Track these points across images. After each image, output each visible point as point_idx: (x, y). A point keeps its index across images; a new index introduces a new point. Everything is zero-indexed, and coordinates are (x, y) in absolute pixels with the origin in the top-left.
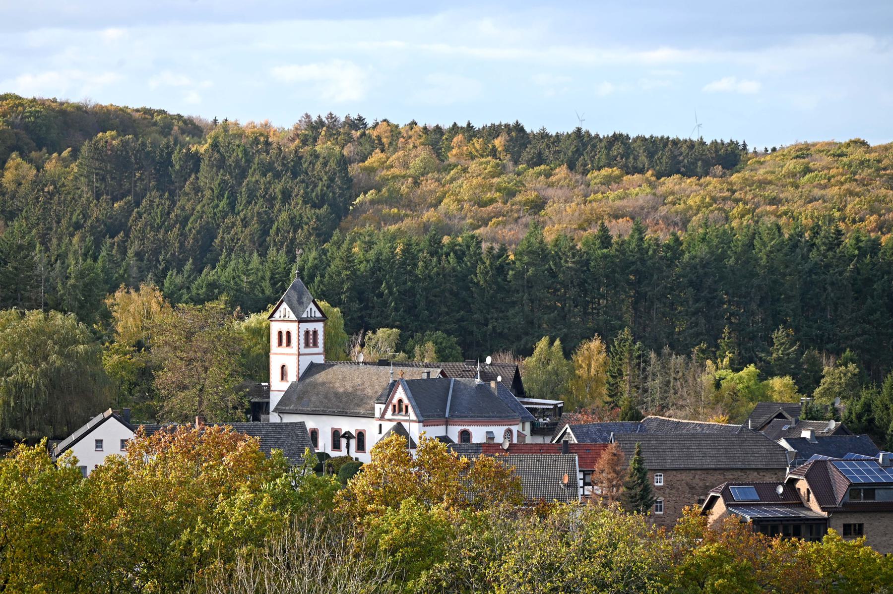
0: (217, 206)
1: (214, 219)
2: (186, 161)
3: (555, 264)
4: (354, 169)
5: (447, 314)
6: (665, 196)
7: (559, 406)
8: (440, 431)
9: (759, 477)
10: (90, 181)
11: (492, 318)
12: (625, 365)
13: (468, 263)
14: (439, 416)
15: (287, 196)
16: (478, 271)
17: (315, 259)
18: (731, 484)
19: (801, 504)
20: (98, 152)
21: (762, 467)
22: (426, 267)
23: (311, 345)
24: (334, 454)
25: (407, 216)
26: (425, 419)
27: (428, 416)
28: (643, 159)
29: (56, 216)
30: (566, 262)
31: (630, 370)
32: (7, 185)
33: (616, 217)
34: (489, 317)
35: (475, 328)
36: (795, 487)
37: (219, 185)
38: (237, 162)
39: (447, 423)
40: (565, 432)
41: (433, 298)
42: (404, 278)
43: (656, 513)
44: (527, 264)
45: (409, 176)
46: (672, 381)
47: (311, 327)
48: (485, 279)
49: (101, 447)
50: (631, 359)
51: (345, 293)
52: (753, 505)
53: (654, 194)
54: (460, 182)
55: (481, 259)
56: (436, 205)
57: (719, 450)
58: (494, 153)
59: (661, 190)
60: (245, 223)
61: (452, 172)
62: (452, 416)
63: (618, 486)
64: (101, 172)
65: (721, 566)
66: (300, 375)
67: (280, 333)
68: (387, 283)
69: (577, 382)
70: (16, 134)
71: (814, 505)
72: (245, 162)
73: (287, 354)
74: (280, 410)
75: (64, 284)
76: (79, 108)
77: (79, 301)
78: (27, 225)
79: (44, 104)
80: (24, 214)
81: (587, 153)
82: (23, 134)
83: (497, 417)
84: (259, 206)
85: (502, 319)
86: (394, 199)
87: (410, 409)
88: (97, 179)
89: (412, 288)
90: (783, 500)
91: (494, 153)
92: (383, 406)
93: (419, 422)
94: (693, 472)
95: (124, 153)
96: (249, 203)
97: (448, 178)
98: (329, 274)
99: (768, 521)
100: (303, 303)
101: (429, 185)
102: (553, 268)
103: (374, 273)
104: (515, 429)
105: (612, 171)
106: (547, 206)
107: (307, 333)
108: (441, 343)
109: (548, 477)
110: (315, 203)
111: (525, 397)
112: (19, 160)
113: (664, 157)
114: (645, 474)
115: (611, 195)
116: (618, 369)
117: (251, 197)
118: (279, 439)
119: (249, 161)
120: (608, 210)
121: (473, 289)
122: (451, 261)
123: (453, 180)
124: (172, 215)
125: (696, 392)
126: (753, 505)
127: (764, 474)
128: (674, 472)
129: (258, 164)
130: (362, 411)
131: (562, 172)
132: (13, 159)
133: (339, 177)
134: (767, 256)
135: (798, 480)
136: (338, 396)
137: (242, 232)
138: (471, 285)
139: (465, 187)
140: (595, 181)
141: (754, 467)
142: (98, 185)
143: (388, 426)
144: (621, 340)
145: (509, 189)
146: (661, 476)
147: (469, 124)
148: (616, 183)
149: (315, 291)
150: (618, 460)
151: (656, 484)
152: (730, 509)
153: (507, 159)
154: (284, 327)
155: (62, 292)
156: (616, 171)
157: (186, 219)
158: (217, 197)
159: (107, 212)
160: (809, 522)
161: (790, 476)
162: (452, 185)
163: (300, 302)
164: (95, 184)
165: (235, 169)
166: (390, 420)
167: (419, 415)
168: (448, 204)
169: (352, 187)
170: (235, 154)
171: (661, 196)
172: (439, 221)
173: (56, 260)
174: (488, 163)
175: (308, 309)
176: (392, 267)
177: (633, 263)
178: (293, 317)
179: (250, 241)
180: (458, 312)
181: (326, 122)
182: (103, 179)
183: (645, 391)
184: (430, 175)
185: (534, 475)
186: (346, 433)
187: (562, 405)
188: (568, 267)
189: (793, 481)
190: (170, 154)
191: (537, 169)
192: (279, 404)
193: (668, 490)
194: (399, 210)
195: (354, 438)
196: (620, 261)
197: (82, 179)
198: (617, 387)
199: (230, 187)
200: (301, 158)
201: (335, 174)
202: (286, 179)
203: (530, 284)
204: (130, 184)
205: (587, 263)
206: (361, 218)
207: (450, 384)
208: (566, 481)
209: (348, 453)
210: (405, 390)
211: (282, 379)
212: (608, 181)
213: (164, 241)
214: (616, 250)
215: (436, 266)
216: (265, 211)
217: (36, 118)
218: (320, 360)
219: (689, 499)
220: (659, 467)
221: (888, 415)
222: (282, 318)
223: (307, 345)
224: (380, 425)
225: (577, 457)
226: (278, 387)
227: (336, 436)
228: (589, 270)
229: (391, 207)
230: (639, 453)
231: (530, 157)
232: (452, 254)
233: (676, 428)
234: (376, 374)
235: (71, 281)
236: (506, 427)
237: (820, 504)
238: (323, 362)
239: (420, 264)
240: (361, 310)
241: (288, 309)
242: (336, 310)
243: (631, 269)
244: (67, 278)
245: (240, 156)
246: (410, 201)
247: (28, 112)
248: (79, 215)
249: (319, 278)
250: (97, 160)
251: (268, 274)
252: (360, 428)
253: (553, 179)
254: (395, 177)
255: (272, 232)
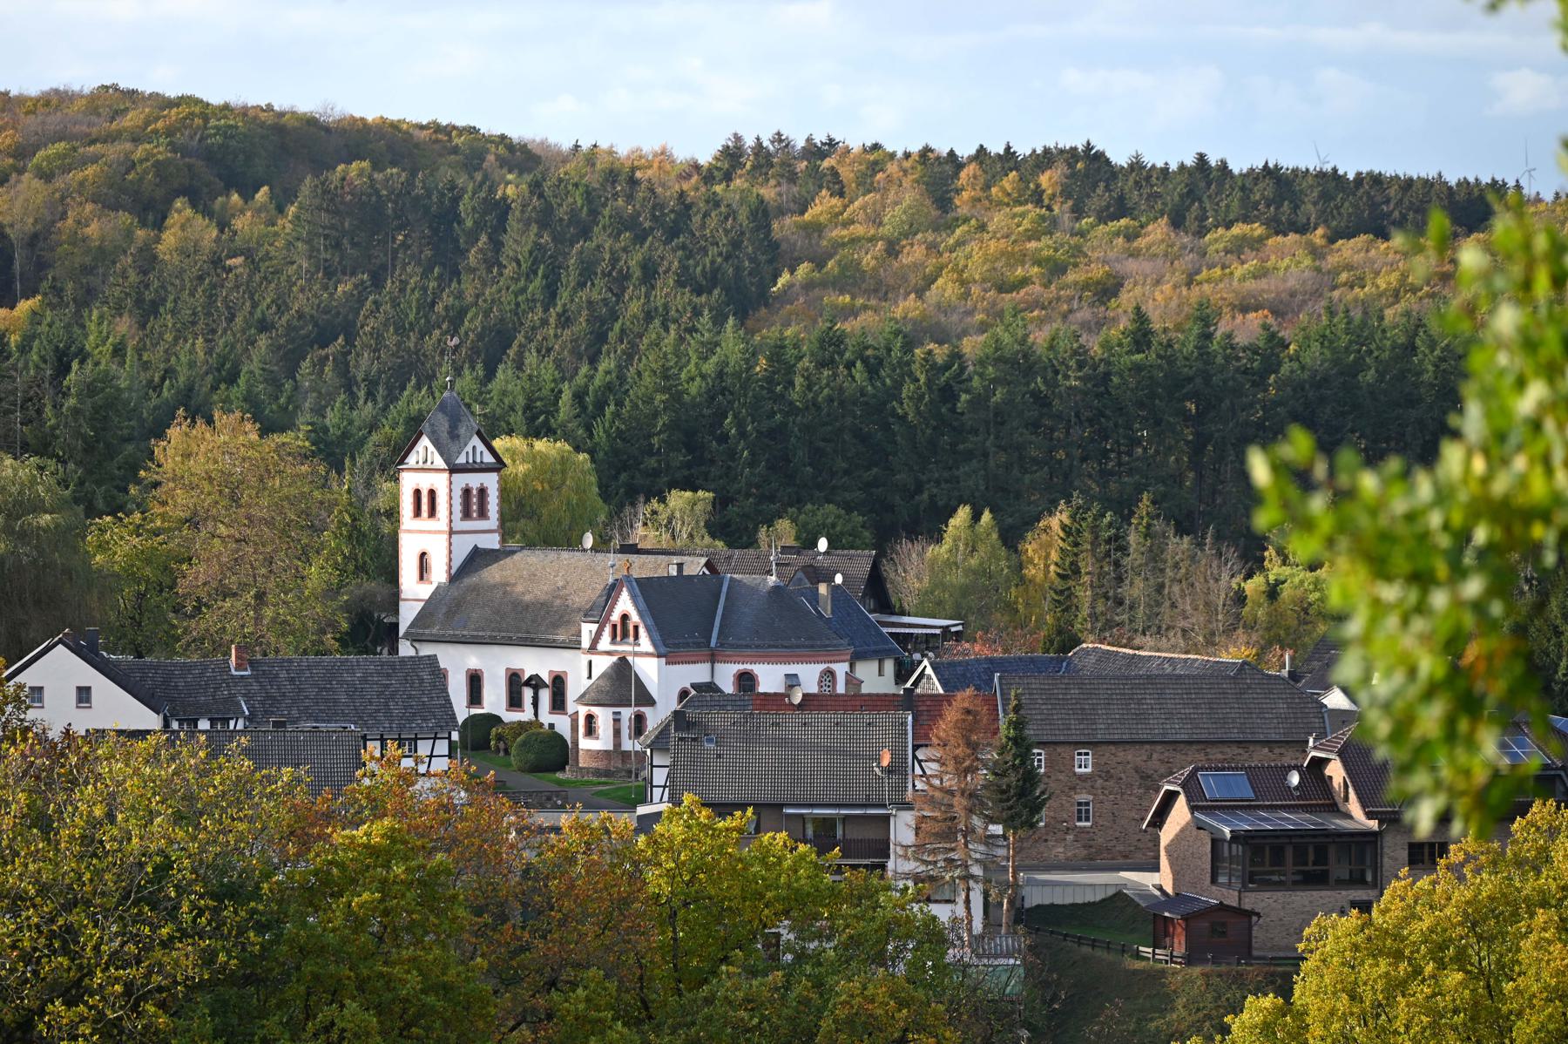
0: (523, 290)
1: (516, 314)
2: (485, 213)
3: (1045, 381)
4: (783, 228)
5: (847, 472)
6: (1335, 272)
7: (953, 629)
8: (697, 673)
9: (1273, 756)
10: (312, 249)
11: (929, 481)
12: (1084, 554)
13: (888, 381)
14: (698, 645)
15: (650, 272)
16: (903, 396)
17: (608, 373)
18: (1202, 769)
19: (1333, 807)
20: (329, 199)
21: (1277, 738)
22: (809, 388)
23: (475, 515)
24: (510, 717)
25: (865, 308)
26: (671, 649)
27: (677, 646)
28: (1309, 209)
29: (228, 308)
30: (1067, 377)
31: (1093, 564)
32: (167, 257)
33: (1245, 309)
34: (924, 478)
35: (897, 499)
36: (1323, 774)
37: (531, 253)
38: (573, 213)
39: (713, 659)
40: (922, 674)
41: (822, 444)
42: (768, 405)
43: (1078, 824)
44: (993, 381)
45: (882, 239)
46: (1167, 584)
47: (474, 480)
48: (917, 408)
49: (88, 700)
50: (1095, 543)
51: (659, 433)
52: (1241, 808)
53: (1318, 270)
54: (968, 249)
55: (911, 374)
56: (920, 293)
57: (1197, 707)
58: (1037, 197)
59: (1332, 260)
60: (565, 320)
61: (958, 232)
62: (722, 645)
63: (972, 770)
64: (334, 233)
65: (388, 867)
66: (453, 572)
67: (417, 493)
68: (735, 417)
69: (1026, 590)
70: (190, 167)
71: (1354, 807)
72: (588, 215)
73: (429, 532)
74: (415, 639)
75: (56, 406)
76: (311, 122)
77: (84, 437)
78: (174, 325)
79: (245, 114)
80: (169, 305)
81: (1210, 197)
82: (199, 164)
83: (807, 647)
84: (597, 292)
85: (947, 481)
86: (850, 279)
87: (642, 632)
88: (325, 246)
89: (784, 425)
90: (1299, 798)
91: (1037, 197)
92: (594, 627)
93: (659, 656)
94: (1148, 747)
95: (374, 199)
96: (582, 285)
97: (951, 241)
98: (631, 401)
99: (1264, 837)
100: (458, 436)
101: (914, 254)
102: (1043, 388)
103: (713, 398)
104: (841, 669)
105: (1252, 229)
106: (1123, 290)
107: (467, 492)
108: (834, 526)
109: (853, 755)
110: (701, 286)
111: (893, 613)
112: (189, 212)
113: (1347, 204)
114: (1029, 749)
115: (1239, 271)
116: (1072, 563)
117: (587, 274)
118: (387, 686)
119: (594, 213)
120: (1230, 296)
121: (895, 428)
122: (858, 376)
123: (960, 243)
124: (439, 308)
125: (1207, 604)
126: (1241, 808)
127: (1283, 751)
128: (1112, 747)
129: (610, 217)
130: (561, 637)
131: (1158, 231)
132: (179, 211)
133: (749, 240)
134: (1437, 366)
135: (1328, 760)
136: (521, 608)
137: (556, 336)
138: (891, 420)
139: (977, 256)
140: (1216, 246)
141: (1262, 737)
142: (328, 257)
143: (602, 664)
144: (1078, 508)
145: (1055, 261)
146: (1087, 754)
147: (1008, 148)
148: (1252, 249)
149: (605, 431)
150: (976, 722)
151: (1077, 770)
152: (1196, 814)
153: (1061, 209)
154: (425, 481)
155: (53, 421)
156: (1258, 229)
157: (462, 313)
158: (528, 275)
159: (321, 302)
160: (1344, 839)
161: (1314, 753)
162: (954, 255)
163: (454, 436)
164: (323, 255)
165: (568, 226)
166: (609, 653)
167: (660, 643)
168: (945, 288)
169: (776, 256)
170: (570, 200)
171: (1329, 272)
172: (924, 317)
173: (163, 379)
174: (1023, 215)
175: (469, 448)
176: (744, 387)
177: (1190, 379)
178: (439, 462)
179: (572, 352)
180: (868, 468)
181: (771, 148)
182: (337, 246)
183: (1119, 602)
184: (919, 236)
185: (828, 751)
186: (531, 678)
187: (960, 628)
188: (1070, 388)
189: (1319, 764)
190: (456, 200)
191: (1114, 225)
192: (412, 625)
193: (1100, 781)
194: (853, 298)
195: (547, 686)
196: (1165, 376)
197: (299, 244)
198: (1069, 597)
199: (550, 257)
200: (688, 207)
201: (743, 233)
202: (652, 243)
203: (1000, 417)
204: (386, 255)
205: (1107, 376)
206: (783, 312)
207: (721, 586)
208: (885, 762)
209: (536, 714)
210: (633, 598)
211: (421, 578)
212: (1238, 248)
213: (416, 353)
214: (1159, 356)
215: (828, 385)
216: (605, 299)
217: (225, 135)
218: (492, 542)
219: (1140, 798)
220: (1083, 739)
221: (1560, 645)
222: (421, 465)
223: (466, 514)
224: (590, 662)
225: (910, 718)
226: (414, 591)
227: (516, 684)
228: (1109, 394)
229: (842, 292)
230: (1016, 709)
231: (1104, 204)
232: (859, 364)
233: (1129, 665)
234: (590, 568)
235: (72, 401)
236: (823, 666)
237: (1364, 805)
238: (497, 547)
239: (798, 380)
240: (688, 465)
241: (431, 448)
242: (582, 457)
243: (1185, 391)
244: (65, 395)
245: (579, 203)
246: (880, 282)
247: (212, 128)
248: (269, 307)
249: (612, 407)
250: (327, 211)
251: (521, 401)
252: (558, 668)
253: (1141, 243)
254: (854, 241)
255: (612, 336)
